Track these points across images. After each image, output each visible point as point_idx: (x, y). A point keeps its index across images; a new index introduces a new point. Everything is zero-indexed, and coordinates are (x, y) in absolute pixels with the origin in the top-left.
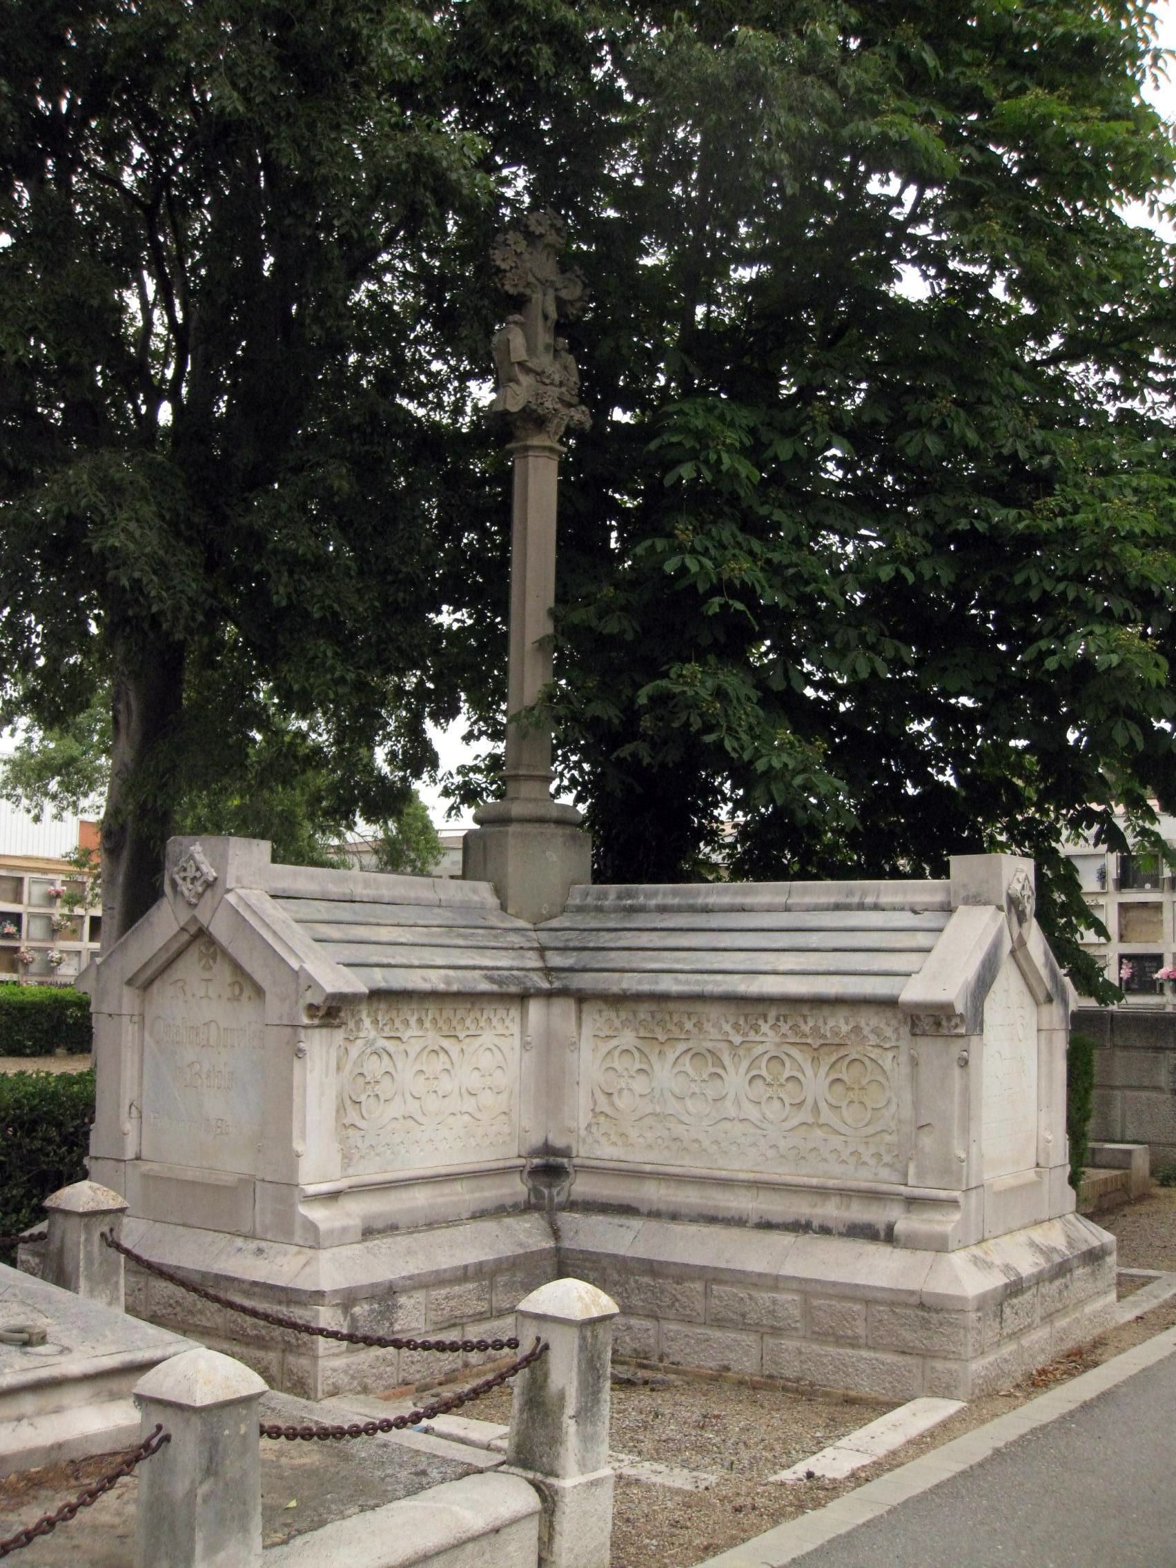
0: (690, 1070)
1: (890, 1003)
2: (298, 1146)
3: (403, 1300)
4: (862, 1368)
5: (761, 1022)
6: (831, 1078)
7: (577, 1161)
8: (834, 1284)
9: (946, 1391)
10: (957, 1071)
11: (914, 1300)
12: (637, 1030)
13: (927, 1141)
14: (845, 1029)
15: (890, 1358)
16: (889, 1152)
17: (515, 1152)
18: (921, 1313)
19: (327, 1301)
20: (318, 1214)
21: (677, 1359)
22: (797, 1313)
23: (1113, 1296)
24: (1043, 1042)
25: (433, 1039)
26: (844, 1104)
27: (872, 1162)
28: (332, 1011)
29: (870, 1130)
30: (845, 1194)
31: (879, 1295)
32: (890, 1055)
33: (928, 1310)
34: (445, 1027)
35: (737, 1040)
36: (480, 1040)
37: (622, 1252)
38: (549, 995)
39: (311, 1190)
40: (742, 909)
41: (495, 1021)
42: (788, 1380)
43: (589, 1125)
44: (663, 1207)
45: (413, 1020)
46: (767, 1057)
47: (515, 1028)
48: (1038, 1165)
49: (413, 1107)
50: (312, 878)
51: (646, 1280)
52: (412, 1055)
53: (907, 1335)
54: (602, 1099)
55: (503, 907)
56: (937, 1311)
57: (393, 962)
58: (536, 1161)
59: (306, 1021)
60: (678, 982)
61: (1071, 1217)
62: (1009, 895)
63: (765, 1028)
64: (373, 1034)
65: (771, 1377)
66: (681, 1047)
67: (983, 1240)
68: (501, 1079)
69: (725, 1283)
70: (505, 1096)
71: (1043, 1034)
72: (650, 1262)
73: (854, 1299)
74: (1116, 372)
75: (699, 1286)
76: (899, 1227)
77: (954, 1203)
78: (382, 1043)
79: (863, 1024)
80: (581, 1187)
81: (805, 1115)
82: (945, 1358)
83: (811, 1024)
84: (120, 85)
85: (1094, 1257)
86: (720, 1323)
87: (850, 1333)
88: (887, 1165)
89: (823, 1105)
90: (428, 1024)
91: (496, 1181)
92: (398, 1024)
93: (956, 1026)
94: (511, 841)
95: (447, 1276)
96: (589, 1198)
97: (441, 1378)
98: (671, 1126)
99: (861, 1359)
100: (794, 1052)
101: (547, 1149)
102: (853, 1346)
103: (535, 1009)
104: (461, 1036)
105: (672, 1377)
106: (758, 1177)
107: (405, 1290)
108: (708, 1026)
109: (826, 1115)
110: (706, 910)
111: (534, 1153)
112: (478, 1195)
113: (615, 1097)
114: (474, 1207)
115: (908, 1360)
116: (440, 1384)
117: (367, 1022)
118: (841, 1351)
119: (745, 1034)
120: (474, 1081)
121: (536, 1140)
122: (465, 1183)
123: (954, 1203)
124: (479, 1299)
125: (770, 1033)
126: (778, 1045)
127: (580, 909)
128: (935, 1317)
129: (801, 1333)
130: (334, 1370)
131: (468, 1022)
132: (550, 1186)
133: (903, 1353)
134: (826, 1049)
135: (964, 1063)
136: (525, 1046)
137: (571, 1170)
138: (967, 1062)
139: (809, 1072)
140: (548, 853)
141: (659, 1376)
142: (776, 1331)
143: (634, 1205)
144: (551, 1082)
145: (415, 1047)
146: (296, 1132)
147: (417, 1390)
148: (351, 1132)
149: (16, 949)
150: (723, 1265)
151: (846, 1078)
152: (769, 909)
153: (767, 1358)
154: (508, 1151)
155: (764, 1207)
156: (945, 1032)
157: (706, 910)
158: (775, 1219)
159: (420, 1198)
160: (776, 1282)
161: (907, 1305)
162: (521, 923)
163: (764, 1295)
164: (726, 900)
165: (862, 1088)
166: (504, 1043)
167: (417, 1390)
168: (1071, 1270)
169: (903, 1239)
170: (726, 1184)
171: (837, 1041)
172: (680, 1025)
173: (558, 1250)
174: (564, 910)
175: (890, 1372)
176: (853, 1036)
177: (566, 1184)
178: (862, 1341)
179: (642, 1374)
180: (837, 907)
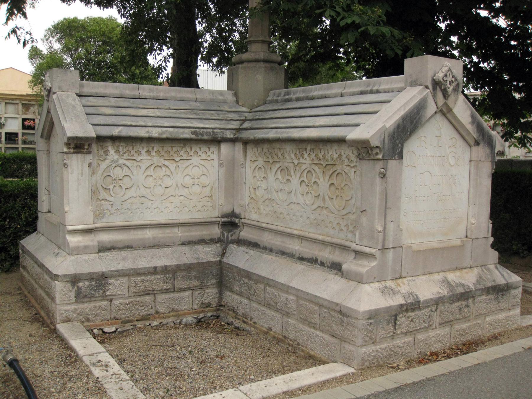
0: (280, 177)
1: (341, 141)
2: (66, 208)
3: (112, 281)
4: (316, 340)
5: (304, 153)
6: (330, 183)
7: (243, 220)
8: (308, 294)
9: (347, 362)
10: (378, 180)
11: (338, 308)
12: (263, 158)
13: (364, 220)
14: (336, 156)
15: (328, 338)
16: (352, 224)
17: (216, 215)
18: (340, 316)
19: (60, 279)
20: (73, 240)
21: (256, 321)
22: (294, 306)
23: (518, 311)
24: (472, 168)
25: (157, 160)
26: (335, 198)
27: (345, 229)
28: (78, 145)
29: (344, 212)
30: (333, 245)
31: (325, 303)
32: (353, 170)
33: (343, 314)
34: (165, 155)
35: (296, 162)
36: (190, 162)
37: (239, 266)
38: (233, 141)
39: (71, 228)
40: (325, 97)
41: (200, 153)
42: (291, 340)
43: (248, 204)
44: (267, 245)
45: (144, 152)
46: (306, 171)
47: (215, 157)
48: (467, 237)
49: (144, 191)
50: (116, 88)
51: (246, 280)
52: (143, 168)
53: (335, 328)
54: (252, 190)
55: (237, 102)
56: (348, 316)
57: (133, 124)
58: (225, 219)
59: (65, 150)
60: (276, 133)
61: (492, 267)
62: (433, 80)
63: (306, 156)
64: (116, 157)
65: (285, 337)
66: (278, 166)
67: (401, 277)
68: (204, 180)
69: (273, 287)
70: (208, 189)
71: (473, 163)
72: (248, 272)
73: (315, 303)
75: (262, 286)
76: (344, 267)
77: (371, 256)
78: (121, 161)
79: (343, 154)
80: (245, 234)
81: (319, 203)
82: (349, 343)
83: (323, 154)
85: (499, 291)
86: (268, 306)
87: (313, 321)
88: (350, 231)
89: (327, 197)
90: (154, 154)
91: (202, 228)
92: (133, 152)
93: (377, 154)
94: (240, 70)
95: (142, 271)
96: (245, 238)
97: (139, 317)
98: (274, 205)
99: (317, 336)
100: (316, 168)
101: (233, 214)
102: (315, 328)
103: (225, 148)
104: (177, 160)
105: (252, 329)
106: (302, 233)
107: (112, 277)
108: (286, 155)
109: (329, 203)
110: (313, 98)
111: (223, 216)
112: (187, 234)
113: (256, 190)
114: (182, 240)
115: (334, 340)
116: (137, 320)
117: (112, 152)
118: (309, 329)
119: (299, 159)
120: (188, 180)
121: (227, 209)
122: (180, 228)
123: (371, 256)
124: (164, 283)
125: (308, 158)
126: (310, 165)
127: (271, 102)
128: (346, 320)
129: (296, 317)
130: (66, 311)
131: (182, 153)
132: (229, 232)
133: (333, 336)
134: (182, 161)
135: (383, 176)
136: (221, 165)
137: (240, 225)
138: (385, 175)
139: (322, 179)
140: (257, 76)
141: (248, 328)
142: (288, 314)
143: (259, 243)
144: (232, 182)
145: (145, 164)
146: (65, 201)
147: (122, 323)
148: (103, 202)
150: (271, 278)
151: (335, 183)
152: (335, 96)
153: (284, 327)
154: (214, 215)
155: (301, 249)
156: (372, 157)
157: (313, 98)
158: (305, 256)
159: (149, 234)
160: (287, 289)
161: (335, 311)
162: (244, 109)
163: (284, 295)
164: (321, 93)
165: (342, 189)
166: (207, 164)
167: (122, 323)
168: (473, 297)
169: (345, 273)
170: (290, 235)
171: (332, 163)
172: (277, 155)
173: (220, 262)
174: (265, 103)
175: (327, 345)
176: (338, 160)
177: (237, 231)
178: (318, 326)
179: (243, 326)
180: (362, 93)
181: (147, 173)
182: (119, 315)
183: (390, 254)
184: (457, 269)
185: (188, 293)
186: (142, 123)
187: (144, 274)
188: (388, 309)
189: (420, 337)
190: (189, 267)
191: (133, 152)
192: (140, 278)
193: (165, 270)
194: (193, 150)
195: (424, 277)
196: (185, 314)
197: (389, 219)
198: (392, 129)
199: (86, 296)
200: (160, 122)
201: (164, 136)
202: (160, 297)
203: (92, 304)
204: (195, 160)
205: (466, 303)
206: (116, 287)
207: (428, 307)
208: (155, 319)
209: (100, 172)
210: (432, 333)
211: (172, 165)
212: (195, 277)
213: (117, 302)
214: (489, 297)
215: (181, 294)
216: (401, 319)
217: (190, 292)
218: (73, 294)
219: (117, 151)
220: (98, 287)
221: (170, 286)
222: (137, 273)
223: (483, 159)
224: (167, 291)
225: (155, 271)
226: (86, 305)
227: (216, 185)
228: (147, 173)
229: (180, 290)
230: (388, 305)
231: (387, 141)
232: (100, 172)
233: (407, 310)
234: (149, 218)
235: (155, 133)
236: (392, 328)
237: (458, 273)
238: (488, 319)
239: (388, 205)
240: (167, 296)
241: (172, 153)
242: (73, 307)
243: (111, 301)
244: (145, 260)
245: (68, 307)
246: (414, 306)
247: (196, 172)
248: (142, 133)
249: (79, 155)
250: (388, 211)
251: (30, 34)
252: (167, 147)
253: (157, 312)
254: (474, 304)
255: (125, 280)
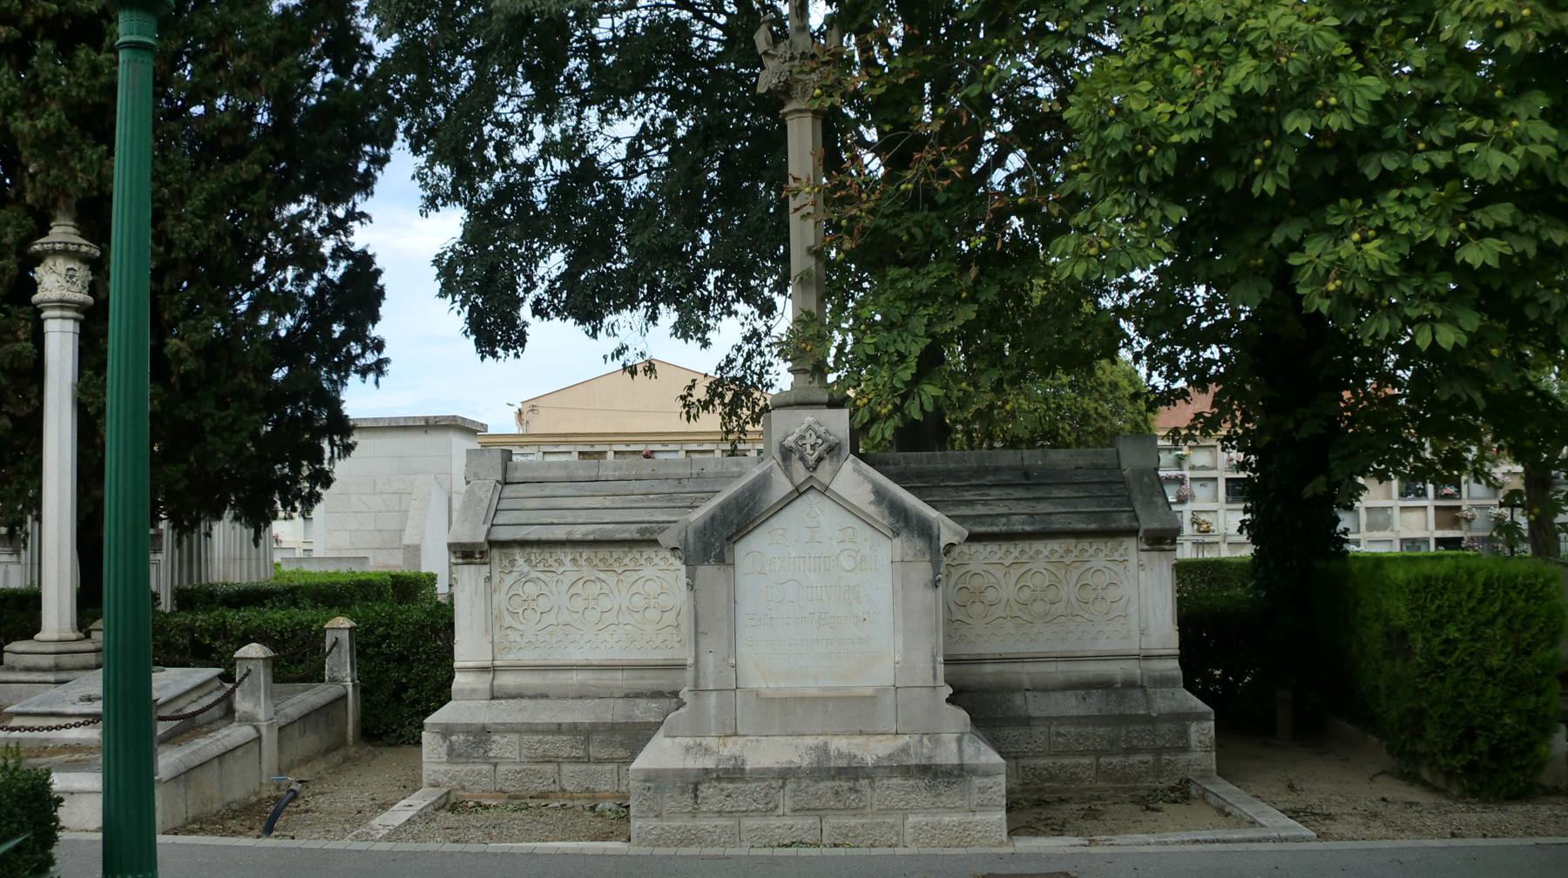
3: (496, 738)
25: (587, 572)
36: (641, 574)
41: (656, 560)
45: (567, 560)
62: (782, 446)
64: (526, 568)
67: (735, 734)
68: (665, 601)
70: (674, 613)
74: (342, 333)
78: (534, 574)
84: (895, 116)
91: (662, 673)
92: (551, 561)
107: (497, 732)
117: (520, 561)
131: (626, 561)
149: (1459, 508)
159: (575, 678)
181: (573, 591)
182: (507, 786)
183: (712, 700)
184: (861, 733)
185: (609, 767)
186: (570, 520)
187: (544, 732)
188: (681, 773)
189: (748, 823)
190: (612, 728)
191: (551, 561)
192: (536, 738)
193: (574, 729)
194: (645, 555)
195: (783, 740)
196: (604, 798)
197: (702, 646)
198: (700, 523)
199: (460, 755)
200: (583, 516)
201: (591, 537)
202: (567, 769)
203: (470, 767)
204: (648, 571)
205: (851, 784)
206: (503, 746)
207: (763, 780)
208: (557, 799)
209: (504, 589)
210: (774, 821)
211: (611, 579)
212: (622, 745)
213: (502, 768)
214: (911, 782)
215: (600, 767)
216: (706, 790)
217: (615, 766)
218: (444, 750)
219: (528, 561)
220: (477, 745)
221: (581, 753)
222: (532, 729)
223: (909, 558)
224: (577, 760)
225: (558, 729)
226: (460, 767)
227: (684, 610)
228: (573, 591)
229: (599, 761)
230: (681, 766)
231: (691, 539)
232: (504, 589)
233: (718, 779)
234: (577, 656)
235: (578, 533)
236: (690, 802)
237: (860, 740)
238: (912, 819)
239: (700, 629)
240: (578, 767)
241: (611, 561)
242: (443, 768)
243: (495, 765)
244: (545, 713)
245: (437, 767)
246: (734, 773)
247: (653, 588)
248: (560, 533)
249: (1156, 553)
250: (701, 637)
251: (633, 371)
252: (603, 553)
253: (563, 790)
254: (873, 789)
255: (514, 738)
